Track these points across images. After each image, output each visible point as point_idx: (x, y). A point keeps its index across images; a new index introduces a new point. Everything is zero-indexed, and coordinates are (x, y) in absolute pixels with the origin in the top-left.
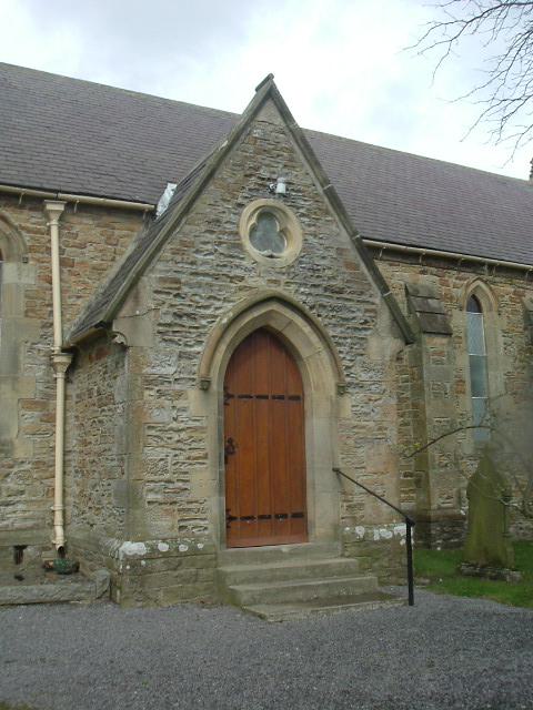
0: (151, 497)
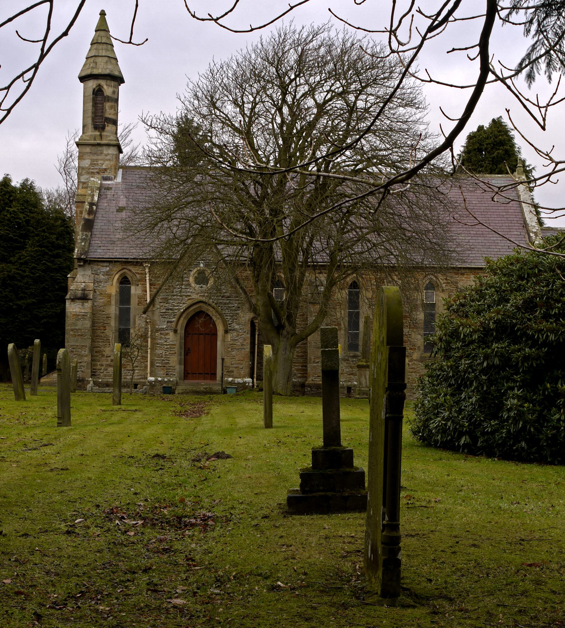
0: (158, 365)
